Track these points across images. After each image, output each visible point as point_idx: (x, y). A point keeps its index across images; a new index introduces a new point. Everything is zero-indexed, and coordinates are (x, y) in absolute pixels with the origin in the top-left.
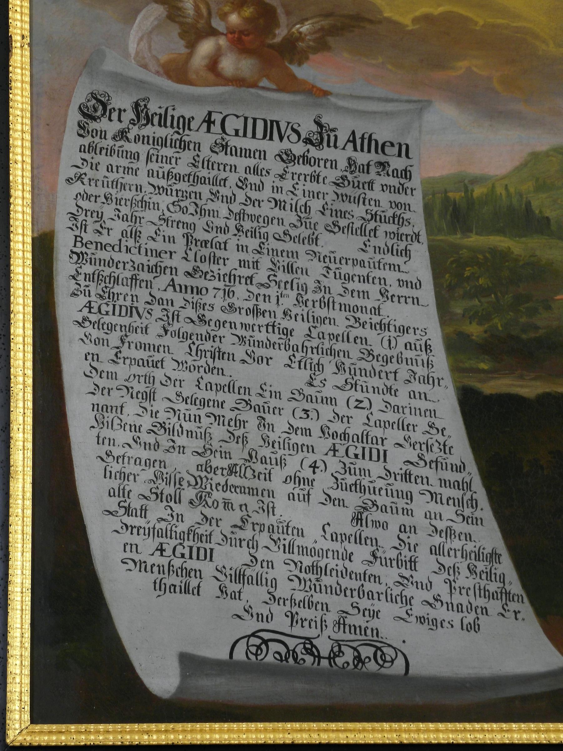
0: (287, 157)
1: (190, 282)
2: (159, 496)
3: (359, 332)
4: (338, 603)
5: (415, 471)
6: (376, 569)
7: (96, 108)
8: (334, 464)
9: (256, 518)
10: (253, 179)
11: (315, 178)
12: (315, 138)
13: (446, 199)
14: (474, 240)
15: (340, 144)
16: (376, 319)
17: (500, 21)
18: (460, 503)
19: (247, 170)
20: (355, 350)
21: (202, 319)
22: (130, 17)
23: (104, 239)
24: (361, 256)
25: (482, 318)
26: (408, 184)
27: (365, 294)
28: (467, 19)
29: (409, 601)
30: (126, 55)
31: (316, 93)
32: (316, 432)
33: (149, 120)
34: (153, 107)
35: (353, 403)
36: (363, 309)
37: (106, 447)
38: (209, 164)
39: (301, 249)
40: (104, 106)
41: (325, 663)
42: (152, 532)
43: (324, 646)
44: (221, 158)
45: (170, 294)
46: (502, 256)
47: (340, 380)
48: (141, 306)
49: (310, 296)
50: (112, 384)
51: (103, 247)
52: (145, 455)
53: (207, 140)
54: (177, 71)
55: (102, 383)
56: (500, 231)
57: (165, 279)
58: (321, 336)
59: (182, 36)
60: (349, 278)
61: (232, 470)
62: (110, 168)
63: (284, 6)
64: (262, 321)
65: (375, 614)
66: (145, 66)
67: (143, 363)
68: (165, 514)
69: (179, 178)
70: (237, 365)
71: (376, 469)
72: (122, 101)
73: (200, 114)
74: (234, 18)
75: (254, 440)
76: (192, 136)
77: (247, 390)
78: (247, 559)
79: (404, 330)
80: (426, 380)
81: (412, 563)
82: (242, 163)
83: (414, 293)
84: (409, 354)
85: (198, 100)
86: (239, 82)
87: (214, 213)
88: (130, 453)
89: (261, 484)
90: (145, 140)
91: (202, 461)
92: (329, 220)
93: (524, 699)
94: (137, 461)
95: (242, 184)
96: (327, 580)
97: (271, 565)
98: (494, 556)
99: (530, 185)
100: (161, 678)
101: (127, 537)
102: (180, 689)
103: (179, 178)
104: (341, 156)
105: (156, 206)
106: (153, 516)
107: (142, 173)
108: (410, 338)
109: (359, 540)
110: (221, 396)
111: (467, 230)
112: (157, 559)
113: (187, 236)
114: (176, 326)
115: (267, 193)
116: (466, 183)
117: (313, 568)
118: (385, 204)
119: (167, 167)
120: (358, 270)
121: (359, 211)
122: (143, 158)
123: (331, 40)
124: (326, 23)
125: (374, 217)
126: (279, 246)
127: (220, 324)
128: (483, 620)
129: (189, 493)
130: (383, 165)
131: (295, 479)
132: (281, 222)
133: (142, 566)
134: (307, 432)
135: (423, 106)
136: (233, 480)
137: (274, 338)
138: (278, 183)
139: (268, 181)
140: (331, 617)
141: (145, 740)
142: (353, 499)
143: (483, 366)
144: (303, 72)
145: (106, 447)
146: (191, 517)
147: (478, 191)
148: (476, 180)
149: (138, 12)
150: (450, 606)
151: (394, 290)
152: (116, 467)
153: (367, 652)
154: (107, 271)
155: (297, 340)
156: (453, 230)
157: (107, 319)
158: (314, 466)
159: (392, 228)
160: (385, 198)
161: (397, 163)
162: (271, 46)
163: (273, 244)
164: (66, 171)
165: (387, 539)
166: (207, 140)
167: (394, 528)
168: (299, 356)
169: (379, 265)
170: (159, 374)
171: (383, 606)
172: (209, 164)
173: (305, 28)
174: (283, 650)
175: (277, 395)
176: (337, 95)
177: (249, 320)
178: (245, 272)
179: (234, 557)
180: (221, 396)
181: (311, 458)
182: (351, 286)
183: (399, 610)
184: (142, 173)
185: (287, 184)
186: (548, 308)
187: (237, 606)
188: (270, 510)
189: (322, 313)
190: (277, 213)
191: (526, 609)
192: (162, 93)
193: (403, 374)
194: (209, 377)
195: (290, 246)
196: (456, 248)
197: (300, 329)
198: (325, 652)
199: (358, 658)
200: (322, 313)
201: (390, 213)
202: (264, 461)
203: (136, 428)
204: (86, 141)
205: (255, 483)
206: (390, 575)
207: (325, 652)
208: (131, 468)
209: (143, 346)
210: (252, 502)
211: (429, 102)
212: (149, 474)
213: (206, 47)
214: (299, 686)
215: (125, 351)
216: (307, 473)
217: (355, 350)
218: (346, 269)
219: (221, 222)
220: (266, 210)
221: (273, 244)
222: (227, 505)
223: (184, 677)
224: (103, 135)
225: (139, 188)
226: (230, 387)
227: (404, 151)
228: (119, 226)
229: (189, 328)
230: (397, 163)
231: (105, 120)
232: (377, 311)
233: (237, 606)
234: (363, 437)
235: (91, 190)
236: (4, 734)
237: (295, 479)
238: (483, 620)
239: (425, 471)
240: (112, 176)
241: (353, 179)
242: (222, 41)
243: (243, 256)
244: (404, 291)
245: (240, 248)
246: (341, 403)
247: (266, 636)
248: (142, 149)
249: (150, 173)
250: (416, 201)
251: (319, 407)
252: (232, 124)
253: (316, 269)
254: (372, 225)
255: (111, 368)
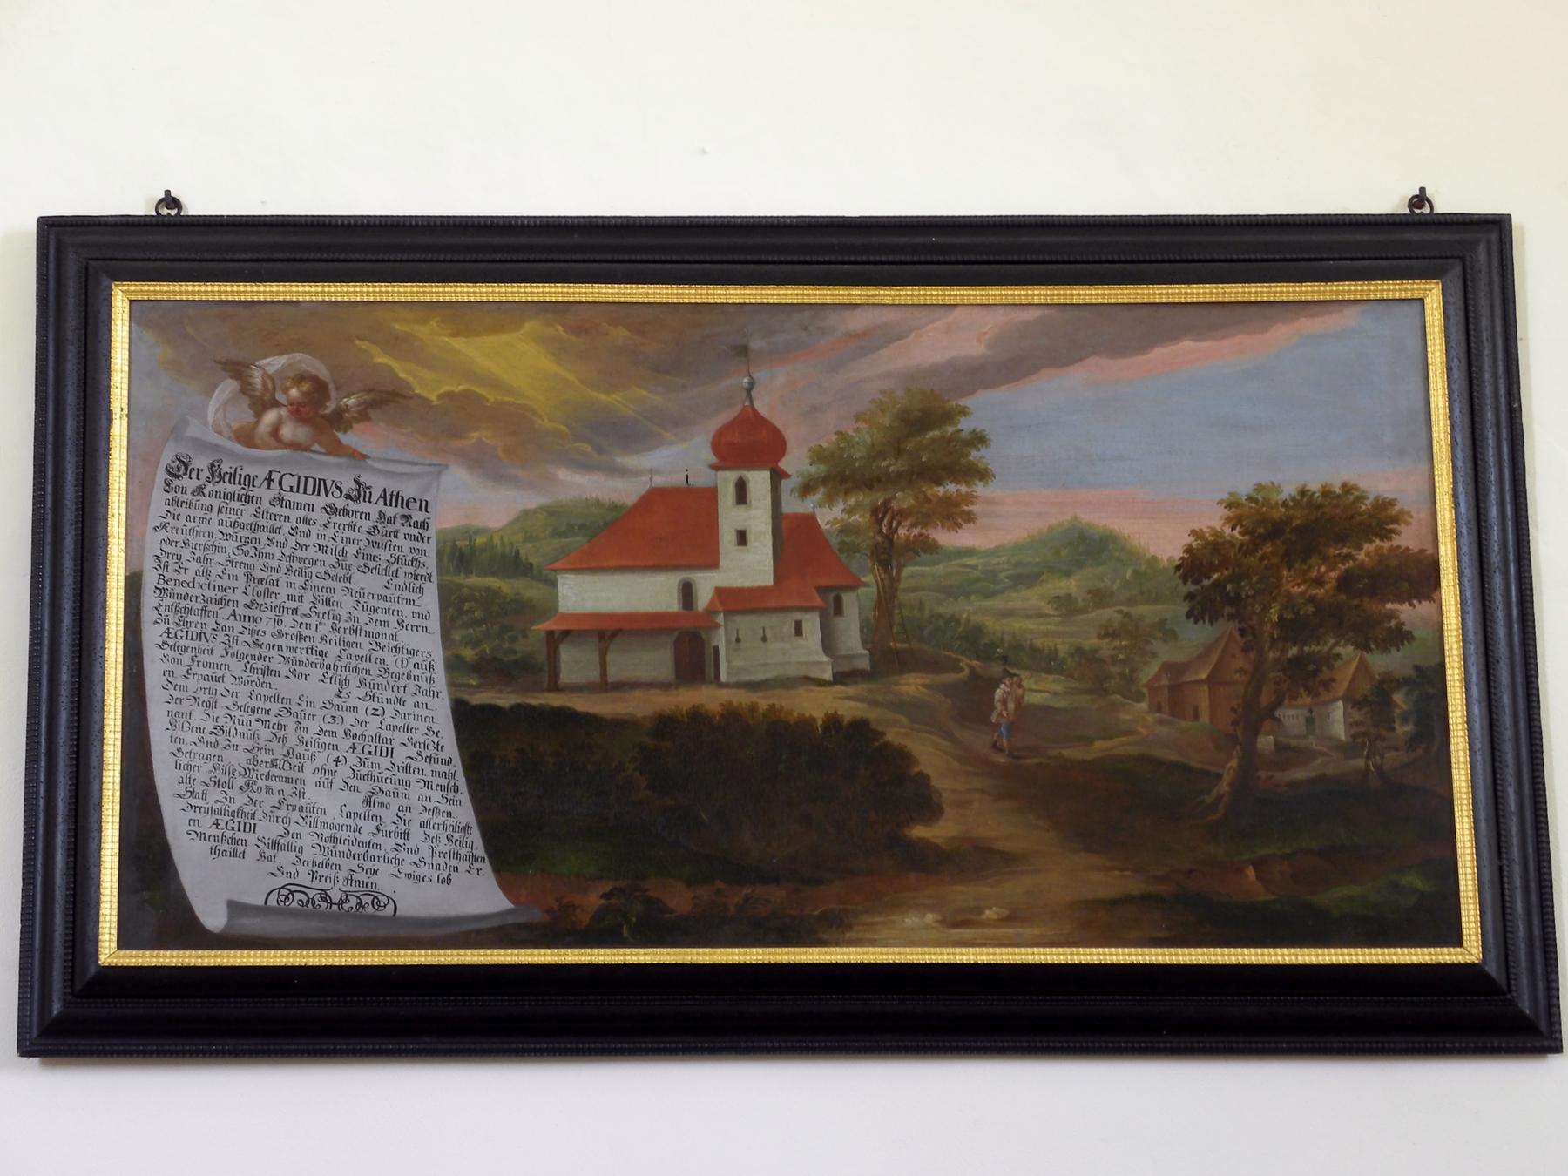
0: (331, 510)
1: (247, 612)
2: (217, 783)
3: (379, 654)
4: (348, 864)
5: (414, 764)
6: (379, 839)
7: (180, 468)
8: (352, 759)
9: (290, 801)
10: (303, 527)
11: (352, 527)
12: (353, 494)
13: (454, 547)
14: (474, 580)
15: (374, 499)
16: (393, 644)
17: (507, 399)
18: (446, 788)
19: (298, 520)
20: (375, 669)
21: (256, 642)
22: (209, 392)
23: (182, 577)
24: (384, 592)
25: (475, 643)
26: (425, 534)
27: (386, 623)
28: (479, 396)
29: (401, 863)
30: (205, 423)
31: (358, 457)
32: (341, 734)
33: (222, 479)
34: (225, 468)
35: (370, 711)
36: (383, 635)
37: (177, 745)
38: (268, 516)
39: (338, 586)
40: (186, 466)
41: (335, 907)
42: (210, 810)
43: (335, 896)
44: (278, 510)
45: (232, 622)
46: (493, 594)
47: (361, 692)
48: (208, 631)
49: (343, 625)
50: (184, 695)
51: (181, 584)
52: (207, 751)
53: (267, 495)
54: (246, 437)
55: (176, 694)
56: (494, 574)
57: (229, 610)
58: (350, 657)
59: (251, 407)
60: (374, 610)
61: (273, 764)
62: (188, 518)
63: (335, 382)
64: (304, 644)
65: (375, 872)
66: (220, 433)
67: (208, 678)
68: (221, 797)
69: (243, 526)
70: (282, 680)
71: (385, 762)
72: (200, 462)
73: (262, 473)
74: (294, 392)
75: (292, 740)
76: (255, 492)
77: (289, 700)
78: (282, 832)
79: (414, 653)
80: (428, 693)
81: (406, 834)
82: (295, 514)
83: (425, 623)
84: (416, 672)
85: (261, 461)
86: (295, 446)
87: (270, 556)
88: (196, 749)
89: (295, 775)
90: (217, 494)
91: (251, 756)
92: (361, 562)
93: (479, 932)
94: (201, 756)
95: (294, 532)
96: (341, 847)
97: (299, 836)
98: (467, 829)
99: (520, 536)
100: (213, 918)
101: (191, 814)
102: (228, 926)
103: (243, 526)
104: (374, 509)
105: (224, 550)
106: (211, 799)
107: (214, 523)
108: (418, 659)
109: (368, 817)
110: (267, 705)
111: (468, 572)
112: (214, 831)
113: (247, 575)
114: (235, 648)
115: (313, 540)
116: (470, 533)
117: (331, 839)
118: (406, 550)
119: (234, 517)
120: (382, 604)
121: (385, 555)
122: (215, 509)
123: (371, 412)
124: (367, 397)
125: (397, 560)
126: (320, 583)
127: (270, 647)
128: (454, 876)
129: (240, 781)
130: (406, 517)
131: (323, 771)
132: (323, 563)
133: (202, 836)
134: (334, 734)
135: (441, 469)
136: (275, 771)
137: (312, 658)
138: (323, 532)
139: (315, 529)
140: (342, 875)
141: (200, 962)
142: (366, 787)
143: (473, 682)
144: (348, 439)
145: (177, 745)
146: (241, 799)
147: (480, 541)
148: (478, 532)
149: (216, 386)
150: (430, 866)
151: (409, 620)
152: (184, 761)
153: (367, 899)
154: (183, 603)
155: (329, 660)
156: (458, 571)
157: (181, 643)
158: (337, 761)
159: (410, 569)
160: (406, 545)
161: (418, 516)
162: (323, 417)
163: (316, 582)
164: (154, 521)
165: (389, 816)
166: (267, 495)
167: (394, 808)
168: (331, 673)
169: (398, 600)
170: (220, 687)
171: (382, 867)
172: (268, 516)
173: (351, 401)
174: (304, 898)
175: (312, 704)
176: (374, 459)
177: (293, 644)
178: (292, 604)
179: (271, 830)
180: (267, 705)
181: (335, 754)
182: (375, 617)
183: (393, 869)
184: (214, 523)
185: (330, 532)
186: (525, 636)
187: (273, 867)
188: (301, 794)
189: (351, 638)
190: (320, 556)
191: (487, 867)
192: (233, 455)
193: (411, 688)
194: (259, 690)
195: (329, 583)
196: (459, 587)
197: (333, 651)
198: (335, 898)
199: (360, 904)
200: (351, 638)
201: (409, 558)
202: (298, 756)
203: (202, 731)
204: (170, 496)
205: (291, 774)
206: (389, 843)
207: (335, 898)
208: (196, 762)
209: (209, 665)
210: (288, 788)
211: (446, 466)
212: (210, 766)
213: (270, 417)
214: (314, 924)
215: (195, 669)
216: (332, 766)
217: (375, 669)
218: (372, 603)
219: (275, 564)
220: (312, 553)
221: (316, 582)
222: (269, 790)
223: (230, 917)
224: (184, 490)
225: (211, 535)
226: (275, 698)
227: (424, 506)
228: (194, 567)
229: (245, 650)
230: (418, 516)
231: (186, 478)
232: (394, 637)
233: (273, 867)
234: (377, 738)
235: (173, 537)
236: (97, 959)
237: (323, 771)
238: (454, 876)
239: (420, 764)
240: (190, 525)
241: (381, 531)
242: (284, 412)
243: (291, 591)
244: (417, 622)
245: (290, 585)
246: (362, 711)
247: (293, 888)
248: (215, 502)
249: (220, 523)
250: (431, 548)
251: (344, 714)
252: (289, 482)
253: (349, 602)
254: (395, 567)
255: (183, 682)
